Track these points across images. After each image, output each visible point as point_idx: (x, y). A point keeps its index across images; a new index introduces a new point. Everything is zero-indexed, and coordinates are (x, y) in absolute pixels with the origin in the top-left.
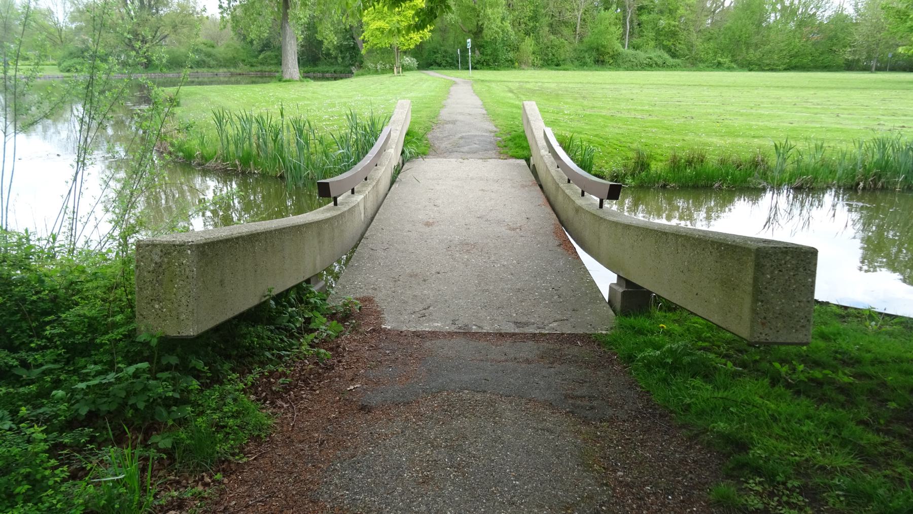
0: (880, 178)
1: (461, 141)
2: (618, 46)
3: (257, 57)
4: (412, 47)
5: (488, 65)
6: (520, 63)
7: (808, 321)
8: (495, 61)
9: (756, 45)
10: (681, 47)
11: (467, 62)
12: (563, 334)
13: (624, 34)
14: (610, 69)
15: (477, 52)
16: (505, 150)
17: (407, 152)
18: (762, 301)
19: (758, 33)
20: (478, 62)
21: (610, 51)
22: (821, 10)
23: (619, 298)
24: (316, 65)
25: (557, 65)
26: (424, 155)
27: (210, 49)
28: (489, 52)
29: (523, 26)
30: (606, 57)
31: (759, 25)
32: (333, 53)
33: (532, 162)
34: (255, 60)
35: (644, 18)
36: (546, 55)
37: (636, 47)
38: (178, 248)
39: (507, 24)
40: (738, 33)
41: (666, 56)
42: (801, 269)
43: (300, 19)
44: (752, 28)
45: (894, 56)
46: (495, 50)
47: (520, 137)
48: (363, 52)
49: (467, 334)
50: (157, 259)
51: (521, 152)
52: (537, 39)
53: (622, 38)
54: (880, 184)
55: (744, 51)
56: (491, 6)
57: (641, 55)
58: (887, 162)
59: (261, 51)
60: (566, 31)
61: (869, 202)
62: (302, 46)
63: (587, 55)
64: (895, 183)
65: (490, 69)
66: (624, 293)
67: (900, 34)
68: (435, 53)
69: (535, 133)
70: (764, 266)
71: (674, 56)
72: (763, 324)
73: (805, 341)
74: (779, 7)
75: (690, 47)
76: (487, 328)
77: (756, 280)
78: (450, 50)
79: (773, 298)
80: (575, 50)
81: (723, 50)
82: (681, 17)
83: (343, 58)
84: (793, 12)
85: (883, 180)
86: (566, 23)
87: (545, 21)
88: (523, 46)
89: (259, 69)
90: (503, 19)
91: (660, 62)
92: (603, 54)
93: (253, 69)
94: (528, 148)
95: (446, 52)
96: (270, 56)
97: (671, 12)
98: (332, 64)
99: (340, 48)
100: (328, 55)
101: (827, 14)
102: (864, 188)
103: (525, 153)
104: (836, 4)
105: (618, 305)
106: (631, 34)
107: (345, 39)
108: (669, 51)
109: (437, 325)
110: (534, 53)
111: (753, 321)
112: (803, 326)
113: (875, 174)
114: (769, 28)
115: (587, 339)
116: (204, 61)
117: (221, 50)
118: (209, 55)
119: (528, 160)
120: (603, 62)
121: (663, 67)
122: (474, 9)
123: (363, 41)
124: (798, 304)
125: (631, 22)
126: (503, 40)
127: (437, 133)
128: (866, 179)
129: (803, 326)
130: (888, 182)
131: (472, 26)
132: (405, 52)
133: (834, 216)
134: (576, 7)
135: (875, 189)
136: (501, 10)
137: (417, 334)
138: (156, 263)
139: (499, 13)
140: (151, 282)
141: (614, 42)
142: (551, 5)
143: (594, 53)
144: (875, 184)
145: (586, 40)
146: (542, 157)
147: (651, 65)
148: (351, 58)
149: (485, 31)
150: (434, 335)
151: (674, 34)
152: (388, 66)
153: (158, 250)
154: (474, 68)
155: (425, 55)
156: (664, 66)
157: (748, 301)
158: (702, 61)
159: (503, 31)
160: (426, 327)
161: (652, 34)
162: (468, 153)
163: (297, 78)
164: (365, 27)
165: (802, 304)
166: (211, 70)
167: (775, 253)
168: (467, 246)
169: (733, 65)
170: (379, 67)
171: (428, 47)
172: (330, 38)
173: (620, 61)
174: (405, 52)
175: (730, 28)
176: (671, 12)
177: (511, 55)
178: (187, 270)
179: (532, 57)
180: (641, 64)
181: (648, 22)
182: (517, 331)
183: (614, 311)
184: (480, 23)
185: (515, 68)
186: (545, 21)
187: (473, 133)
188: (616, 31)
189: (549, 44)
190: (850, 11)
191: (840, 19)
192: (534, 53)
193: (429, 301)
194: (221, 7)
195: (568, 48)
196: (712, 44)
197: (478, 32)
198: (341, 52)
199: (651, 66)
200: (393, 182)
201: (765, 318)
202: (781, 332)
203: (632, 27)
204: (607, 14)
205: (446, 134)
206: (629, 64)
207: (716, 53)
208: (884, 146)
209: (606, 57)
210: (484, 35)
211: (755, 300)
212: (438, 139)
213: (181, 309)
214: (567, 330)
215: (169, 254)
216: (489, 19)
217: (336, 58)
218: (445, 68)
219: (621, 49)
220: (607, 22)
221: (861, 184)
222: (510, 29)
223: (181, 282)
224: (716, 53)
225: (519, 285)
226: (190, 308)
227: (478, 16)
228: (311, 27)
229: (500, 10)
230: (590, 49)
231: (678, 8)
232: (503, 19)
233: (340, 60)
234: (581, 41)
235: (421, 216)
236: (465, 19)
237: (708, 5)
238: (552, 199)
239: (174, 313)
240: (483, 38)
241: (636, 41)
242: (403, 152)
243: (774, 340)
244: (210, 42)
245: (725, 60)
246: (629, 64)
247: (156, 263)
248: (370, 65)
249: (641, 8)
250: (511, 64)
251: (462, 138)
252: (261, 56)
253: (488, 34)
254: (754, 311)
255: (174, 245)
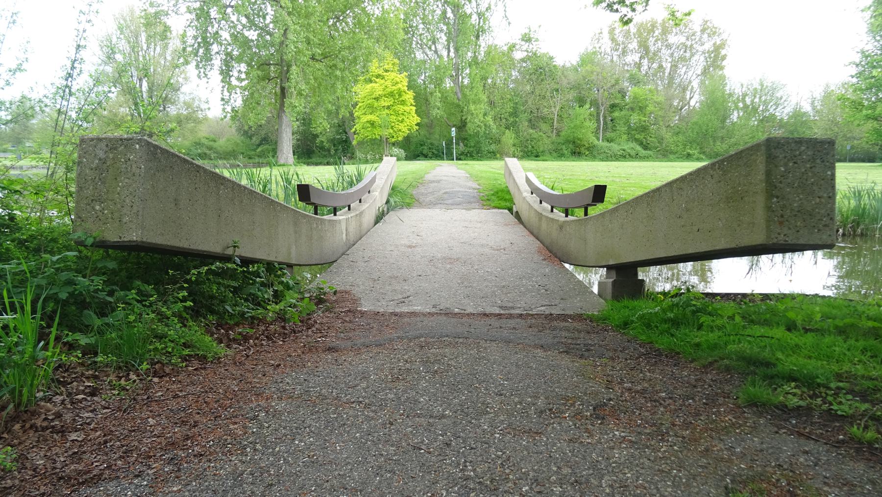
0: (858, 224)
1: (445, 196)
2: (592, 139)
3: (255, 150)
4: (400, 139)
5: (472, 156)
6: (501, 155)
7: (831, 219)
8: (478, 153)
9: (722, 138)
10: (652, 140)
11: (452, 154)
12: (551, 314)
13: (598, 128)
14: (586, 160)
15: (461, 144)
16: (488, 203)
17: (392, 200)
18: (777, 197)
19: (723, 128)
20: (463, 153)
21: (586, 143)
22: (780, 107)
23: (610, 286)
24: (310, 157)
25: (537, 156)
26: (409, 206)
27: (211, 143)
28: (473, 144)
29: (504, 121)
30: (582, 149)
31: (723, 121)
32: (326, 145)
33: (515, 210)
34: (253, 153)
35: (616, 114)
36: (526, 147)
37: (609, 140)
38: (125, 142)
39: (489, 118)
40: (704, 128)
41: (639, 148)
42: (818, 161)
43: (296, 107)
44: (717, 123)
45: (852, 147)
46: (478, 142)
47: (502, 191)
48: (354, 143)
49: (448, 314)
50: (101, 155)
51: (503, 204)
52: (517, 133)
53: (596, 132)
54: (859, 230)
55: (712, 143)
56: (474, 103)
57: (615, 147)
58: (864, 209)
59: (259, 145)
60: (544, 127)
61: (851, 244)
62: (298, 140)
63: (564, 147)
64: (874, 230)
65: (474, 159)
66: (614, 283)
67: (856, 122)
68: (422, 145)
69: (518, 181)
70: (776, 157)
71: (646, 148)
72: (781, 223)
73: (829, 242)
74: (741, 105)
75: (661, 140)
76: (470, 310)
77: (768, 174)
78: (436, 143)
79: (790, 193)
80: (553, 143)
81: (691, 142)
82: (651, 113)
83: (336, 150)
84: (755, 110)
85: (862, 227)
86: (544, 119)
87: (524, 117)
88: (504, 139)
89: (257, 161)
90: (485, 114)
91: (633, 153)
92: (579, 146)
93: (251, 161)
94: (511, 200)
95: (432, 144)
96: (267, 149)
97: (641, 109)
98: (325, 156)
99: (332, 141)
100: (322, 148)
101: (786, 111)
102: (844, 235)
103: (508, 204)
104: (794, 103)
105: (609, 297)
106: (605, 130)
107: (338, 133)
108: (641, 144)
109: (418, 308)
110: (514, 145)
111: (768, 221)
112: (825, 226)
113: (854, 221)
114: (733, 124)
115: (579, 317)
116: (205, 154)
117: (222, 143)
118: (210, 148)
119: (510, 210)
120: (579, 153)
121: (636, 158)
122: (458, 106)
123: (355, 133)
124: (818, 200)
125: (605, 117)
126: (485, 133)
127: (422, 190)
128: (845, 226)
129: (825, 226)
130: (867, 229)
131: (456, 120)
132: (394, 144)
133: (816, 263)
134: (552, 104)
135: (855, 235)
136: (484, 107)
137: (395, 314)
138: (100, 159)
139: (481, 109)
140: (93, 180)
141: (588, 134)
142: (530, 103)
143: (570, 146)
144: (855, 231)
145: (563, 134)
146: (524, 198)
147: (624, 157)
148: (343, 150)
149: (469, 125)
150: (413, 314)
151: (644, 129)
152: (377, 156)
153: (103, 145)
154: (458, 159)
155: (412, 148)
156: (636, 157)
157: (760, 200)
158: (672, 153)
159: (485, 125)
160: (405, 309)
161: (624, 129)
162: (452, 205)
163: (291, 163)
164: (356, 121)
165: (823, 200)
166: (211, 162)
167: (788, 143)
168: (448, 260)
169: (701, 156)
170: (369, 157)
171: (414, 140)
172: (323, 126)
173: (595, 153)
174: (394, 144)
175: (696, 123)
176: (641, 109)
177: (493, 147)
178: (134, 166)
179: (512, 149)
180: (615, 156)
181: (620, 118)
182: (502, 312)
183: (605, 300)
184: (464, 118)
185: (497, 159)
186: (524, 117)
187: (457, 189)
188: (591, 125)
189: (528, 137)
190: (807, 108)
191: (797, 114)
192: (514, 145)
193: (408, 294)
194: (223, 99)
195: (547, 141)
196: (681, 137)
197: (462, 126)
198: (334, 145)
199: (625, 157)
200: (377, 222)
201: (782, 216)
202: (801, 232)
203: (605, 123)
204: (582, 110)
205: (430, 190)
206: (604, 155)
207: (685, 146)
208: (859, 194)
209: (582, 149)
210: (467, 128)
211: (770, 195)
212: (422, 194)
213: (125, 211)
214: (556, 311)
215: (115, 149)
216: (472, 114)
217: (329, 150)
218: (431, 158)
219: (596, 142)
220: (582, 117)
221: (841, 231)
222: (492, 123)
223: (126, 180)
224: (685, 146)
225: (504, 284)
226: (135, 209)
227: (462, 112)
228: (306, 121)
229: (482, 106)
230: (567, 141)
231: (647, 106)
232: (485, 114)
233: (333, 152)
234: (558, 135)
235: (405, 242)
236: (450, 114)
237: (675, 104)
238: (535, 232)
239: (116, 215)
240: (466, 131)
241: (609, 135)
242: (388, 202)
243: (795, 242)
244: (212, 136)
245: (695, 152)
246: (604, 155)
247: (100, 159)
248: (358, 154)
249: (613, 106)
250: (493, 155)
251: (446, 193)
252: (259, 149)
253: (471, 128)
254: (769, 208)
255: (121, 139)
